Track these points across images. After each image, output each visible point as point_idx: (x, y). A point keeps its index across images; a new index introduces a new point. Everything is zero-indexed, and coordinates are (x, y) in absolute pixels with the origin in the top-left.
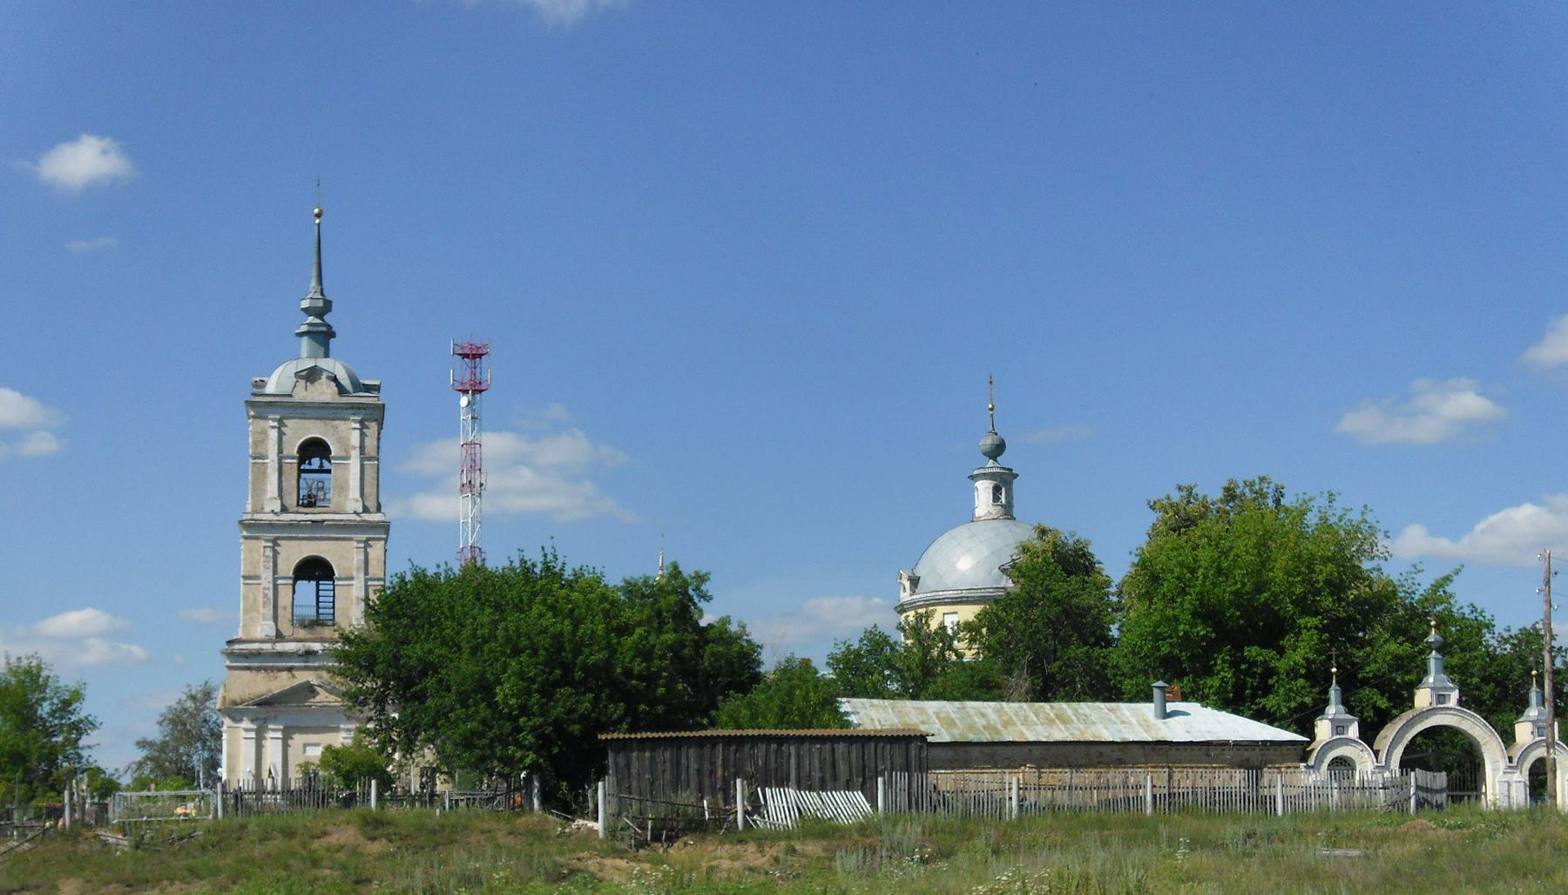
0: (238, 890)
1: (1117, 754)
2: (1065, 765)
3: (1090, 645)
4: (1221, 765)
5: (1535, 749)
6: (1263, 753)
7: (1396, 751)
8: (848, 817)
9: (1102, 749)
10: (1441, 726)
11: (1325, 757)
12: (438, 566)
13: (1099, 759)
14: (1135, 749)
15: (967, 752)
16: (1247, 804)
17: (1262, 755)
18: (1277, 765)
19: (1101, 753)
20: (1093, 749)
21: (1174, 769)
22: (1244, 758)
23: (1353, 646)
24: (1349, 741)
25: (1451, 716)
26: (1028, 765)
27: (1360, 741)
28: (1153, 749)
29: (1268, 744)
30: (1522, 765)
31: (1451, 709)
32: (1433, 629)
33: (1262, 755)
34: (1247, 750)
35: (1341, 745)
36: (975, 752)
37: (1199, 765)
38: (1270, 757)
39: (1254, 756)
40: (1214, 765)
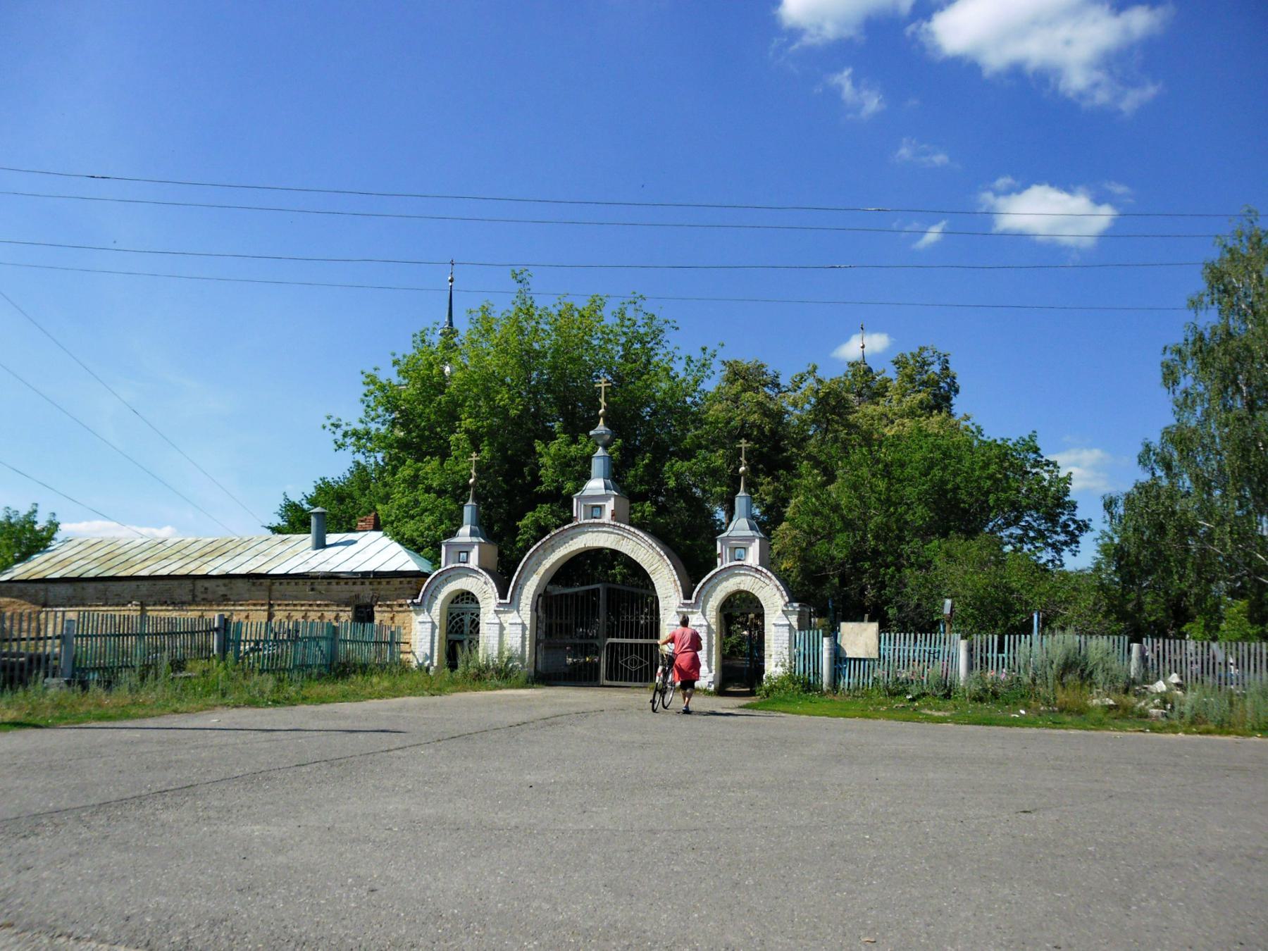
0: (1172, 630)
1: (222, 590)
2: (169, 603)
3: (1206, 595)
4: (326, 602)
5: (727, 579)
6: (375, 587)
7: (528, 583)
8: (89, 657)
9: (207, 584)
10: (621, 552)
11: (440, 592)
12: (315, 482)
13: (205, 596)
14: (240, 584)
15: (83, 589)
16: (811, 637)
17: (373, 590)
18: (388, 603)
19: (206, 589)
20: (200, 583)
21: (276, 608)
22: (353, 594)
23: (1039, 551)
24: (469, 572)
25: (606, 535)
26: (134, 602)
27: (480, 571)
28: (254, 584)
29: (372, 576)
30: (706, 603)
31: (603, 525)
32: (602, 419)
33: (373, 590)
34: (346, 583)
35: (460, 576)
36: (91, 587)
37: (295, 602)
38: (382, 593)
39: (366, 591)
40: (318, 602)
